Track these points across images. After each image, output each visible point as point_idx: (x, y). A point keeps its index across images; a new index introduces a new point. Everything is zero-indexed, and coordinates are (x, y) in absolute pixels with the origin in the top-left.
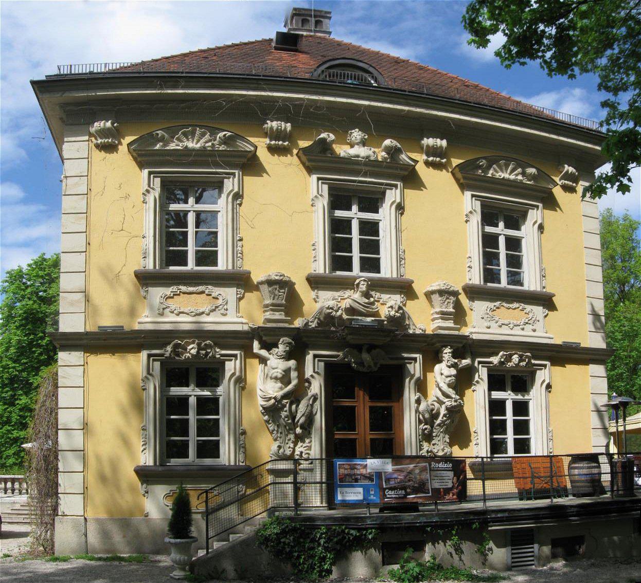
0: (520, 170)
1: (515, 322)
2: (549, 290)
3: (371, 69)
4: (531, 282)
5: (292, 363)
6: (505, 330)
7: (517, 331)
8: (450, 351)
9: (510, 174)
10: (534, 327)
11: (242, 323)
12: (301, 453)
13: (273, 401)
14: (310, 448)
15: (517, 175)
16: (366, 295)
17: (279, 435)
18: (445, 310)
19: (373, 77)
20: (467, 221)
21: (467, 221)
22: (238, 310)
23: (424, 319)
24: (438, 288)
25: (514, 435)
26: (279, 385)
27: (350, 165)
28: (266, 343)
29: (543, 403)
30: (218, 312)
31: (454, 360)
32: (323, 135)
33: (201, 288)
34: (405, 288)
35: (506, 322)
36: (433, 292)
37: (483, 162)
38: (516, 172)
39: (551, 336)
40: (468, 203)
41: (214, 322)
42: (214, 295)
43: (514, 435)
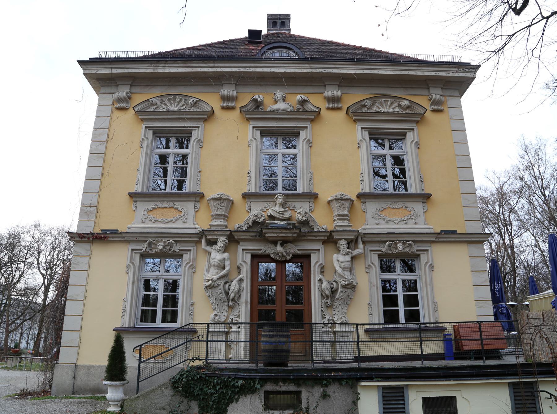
0: (396, 104)
1: (400, 219)
2: (427, 191)
3: (293, 48)
4: (413, 187)
5: (226, 255)
6: (392, 226)
7: (402, 225)
8: (344, 243)
9: (389, 108)
10: (415, 221)
11: (196, 228)
12: (232, 319)
13: (210, 282)
14: (239, 316)
15: (394, 108)
16: (282, 205)
17: (216, 306)
18: (341, 213)
19: (294, 52)
20: (359, 148)
21: (359, 148)
22: (195, 219)
23: (323, 220)
24: (335, 197)
25: (398, 310)
26: (216, 270)
27: (273, 116)
28: (210, 241)
29: (297, 333)
30: (180, 221)
31: (348, 250)
32: (256, 97)
33: (171, 204)
34: (313, 197)
35: (392, 219)
36: (332, 201)
37: (368, 102)
38: (394, 106)
39: (431, 227)
40: (358, 133)
41: (178, 226)
42: (179, 209)
43: (398, 310)
